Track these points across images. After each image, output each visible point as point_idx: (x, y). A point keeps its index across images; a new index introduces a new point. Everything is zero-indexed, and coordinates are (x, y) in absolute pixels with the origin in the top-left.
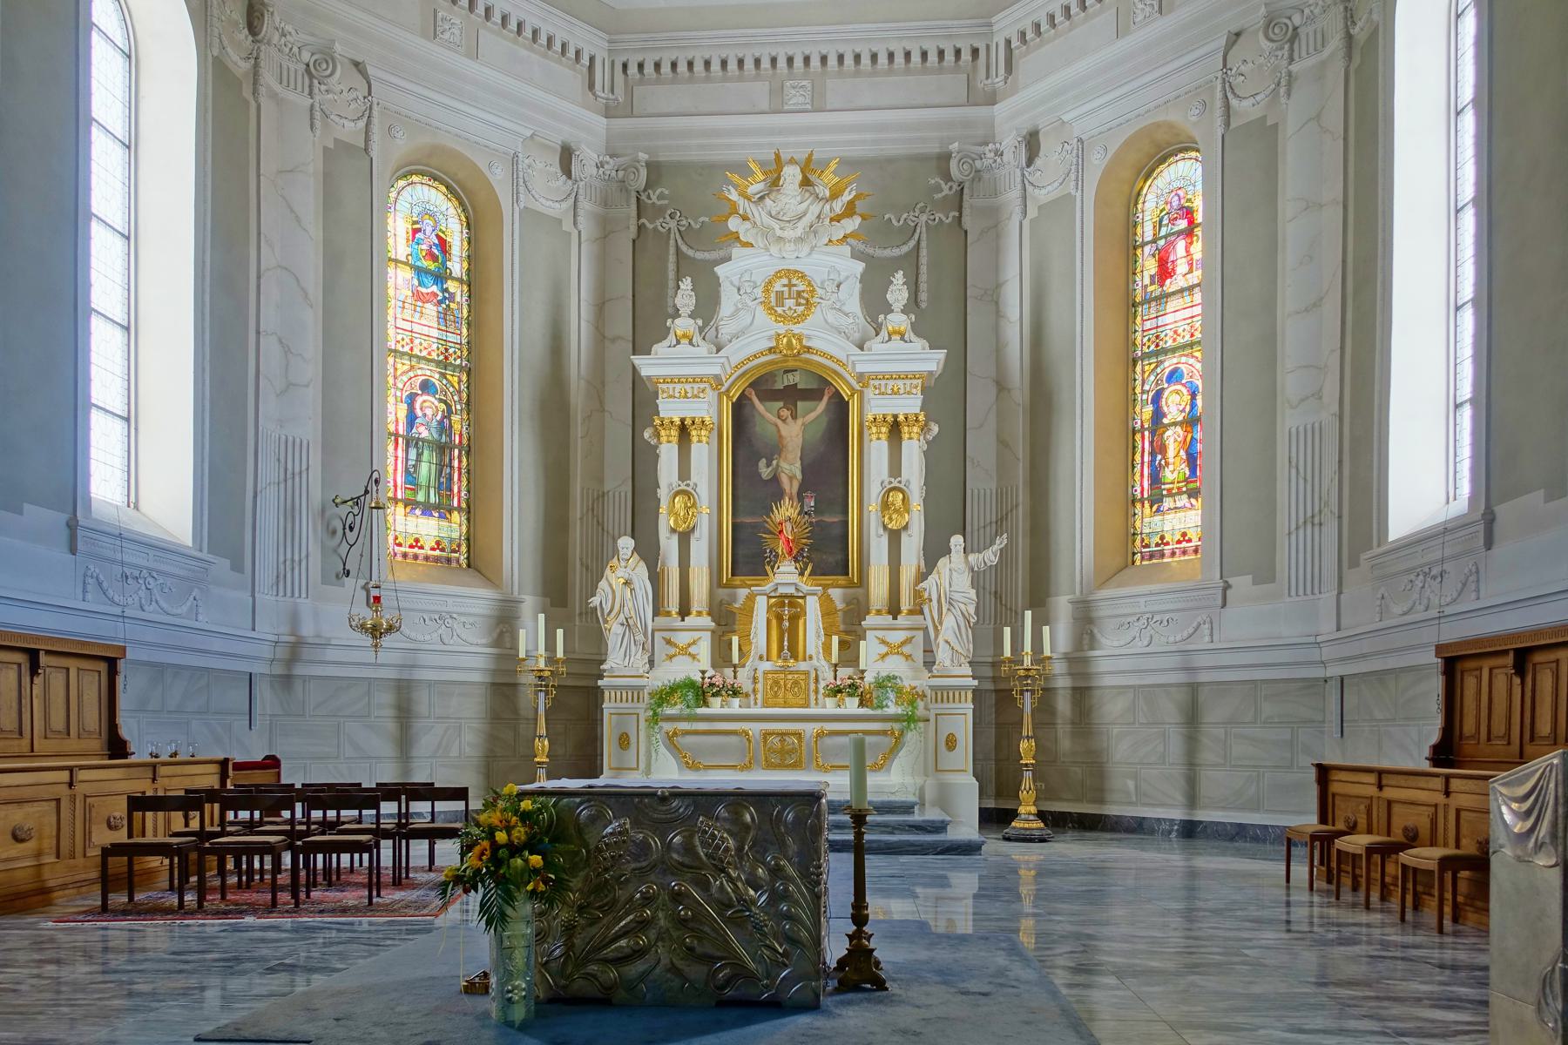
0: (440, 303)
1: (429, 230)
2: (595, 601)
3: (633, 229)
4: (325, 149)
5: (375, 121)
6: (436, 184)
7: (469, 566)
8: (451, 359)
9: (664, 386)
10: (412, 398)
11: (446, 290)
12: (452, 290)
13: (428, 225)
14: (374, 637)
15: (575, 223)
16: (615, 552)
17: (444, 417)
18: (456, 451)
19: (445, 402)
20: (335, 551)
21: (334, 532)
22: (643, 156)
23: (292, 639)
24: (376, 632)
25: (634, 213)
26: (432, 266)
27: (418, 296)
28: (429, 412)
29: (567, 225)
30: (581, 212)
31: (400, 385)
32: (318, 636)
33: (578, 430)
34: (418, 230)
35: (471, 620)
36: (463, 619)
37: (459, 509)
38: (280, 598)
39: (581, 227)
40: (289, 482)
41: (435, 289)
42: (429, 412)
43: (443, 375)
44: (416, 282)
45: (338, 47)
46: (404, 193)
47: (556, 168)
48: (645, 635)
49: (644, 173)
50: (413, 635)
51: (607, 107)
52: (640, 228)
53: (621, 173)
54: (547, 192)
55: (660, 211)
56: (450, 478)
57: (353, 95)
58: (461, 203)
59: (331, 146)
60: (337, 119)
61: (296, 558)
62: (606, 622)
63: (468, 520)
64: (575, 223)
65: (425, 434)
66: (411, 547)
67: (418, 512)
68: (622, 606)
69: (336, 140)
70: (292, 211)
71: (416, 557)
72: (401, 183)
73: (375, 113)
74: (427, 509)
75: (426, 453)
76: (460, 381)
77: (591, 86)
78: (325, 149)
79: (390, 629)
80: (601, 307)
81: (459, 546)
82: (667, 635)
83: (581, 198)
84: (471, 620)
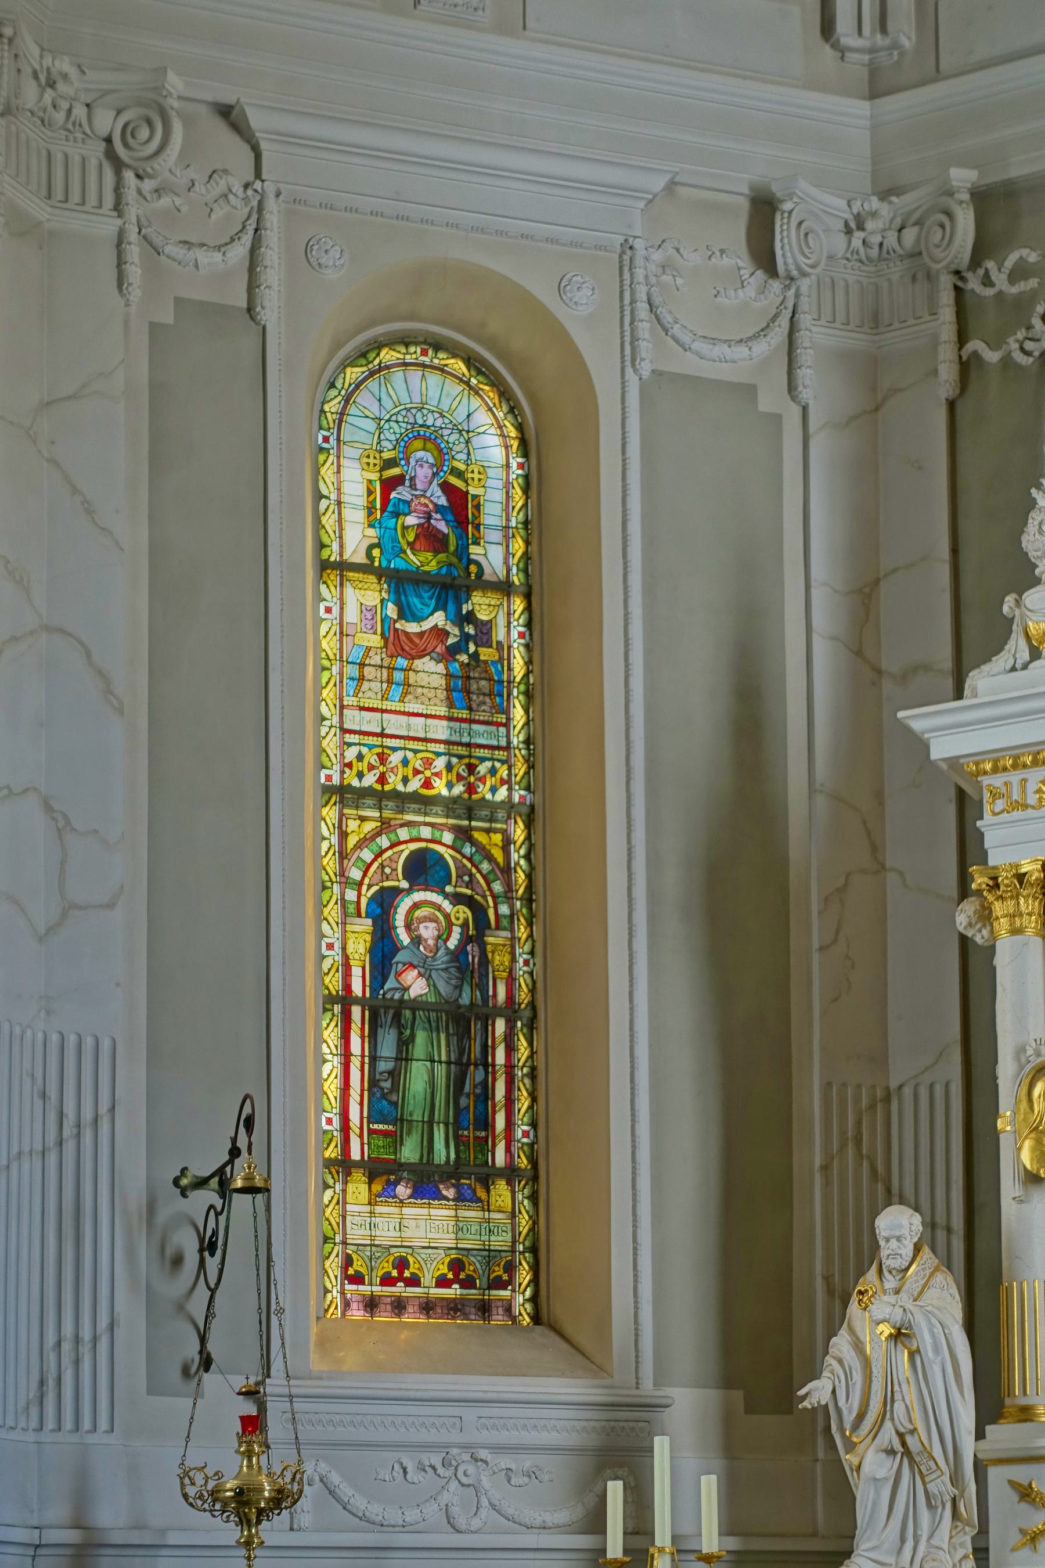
0: (452, 652)
1: (423, 473)
2: (817, 1392)
3: (948, 373)
4: (154, 328)
5: (272, 237)
6: (442, 358)
7: (536, 1319)
8: (484, 791)
9: (997, 781)
10: (384, 902)
11: (470, 618)
12: (483, 616)
13: (421, 465)
14: (244, 1521)
15: (792, 387)
16: (868, 1253)
17: (466, 939)
18: (500, 1026)
19: (469, 902)
20: (180, 1307)
21: (177, 1261)
22: (963, 177)
23: (72, 1536)
24: (246, 1507)
25: (948, 331)
26: (426, 562)
27: (397, 645)
28: (428, 932)
29: (771, 398)
30: (806, 356)
31: (356, 874)
32: (139, 1526)
33: (811, 928)
34: (398, 481)
35: (528, 1462)
36: (505, 1461)
37: (511, 1173)
38: (46, 1437)
39: (806, 394)
40: (69, 1147)
41: (439, 619)
42: (428, 932)
43: (464, 835)
44: (391, 611)
45: (175, 82)
46: (363, 398)
47: (738, 258)
48: (956, 1478)
49: (966, 221)
50: (375, 1511)
51: (874, 72)
52: (967, 368)
53: (910, 235)
54: (716, 322)
55: (1017, 310)
56: (486, 1094)
57: (221, 184)
58: (505, 395)
59: (167, 318)
60: (179, 252)
61: (86, 1334)
62: (850, 1447)
63: (534, 1198)
64: (792, 387)
65: (417, 987)
66: (387, 1281)
67: (402, 1190)
68: (889, 1401)
69: (179, 302)
70: (75, 490)
71: (399, 1306)
72: (353, 373)
73: (273, 218)
74: (426, 1183)
75: (421, 1037)
76: (507, 843)
77: (827, 28)
78: (154, 328)
79: (281, 1499)
80: (864, 597)
81: (511, 1268)
82: (1021, 1473)
83: (805, 320)
84: (528, 1462)
